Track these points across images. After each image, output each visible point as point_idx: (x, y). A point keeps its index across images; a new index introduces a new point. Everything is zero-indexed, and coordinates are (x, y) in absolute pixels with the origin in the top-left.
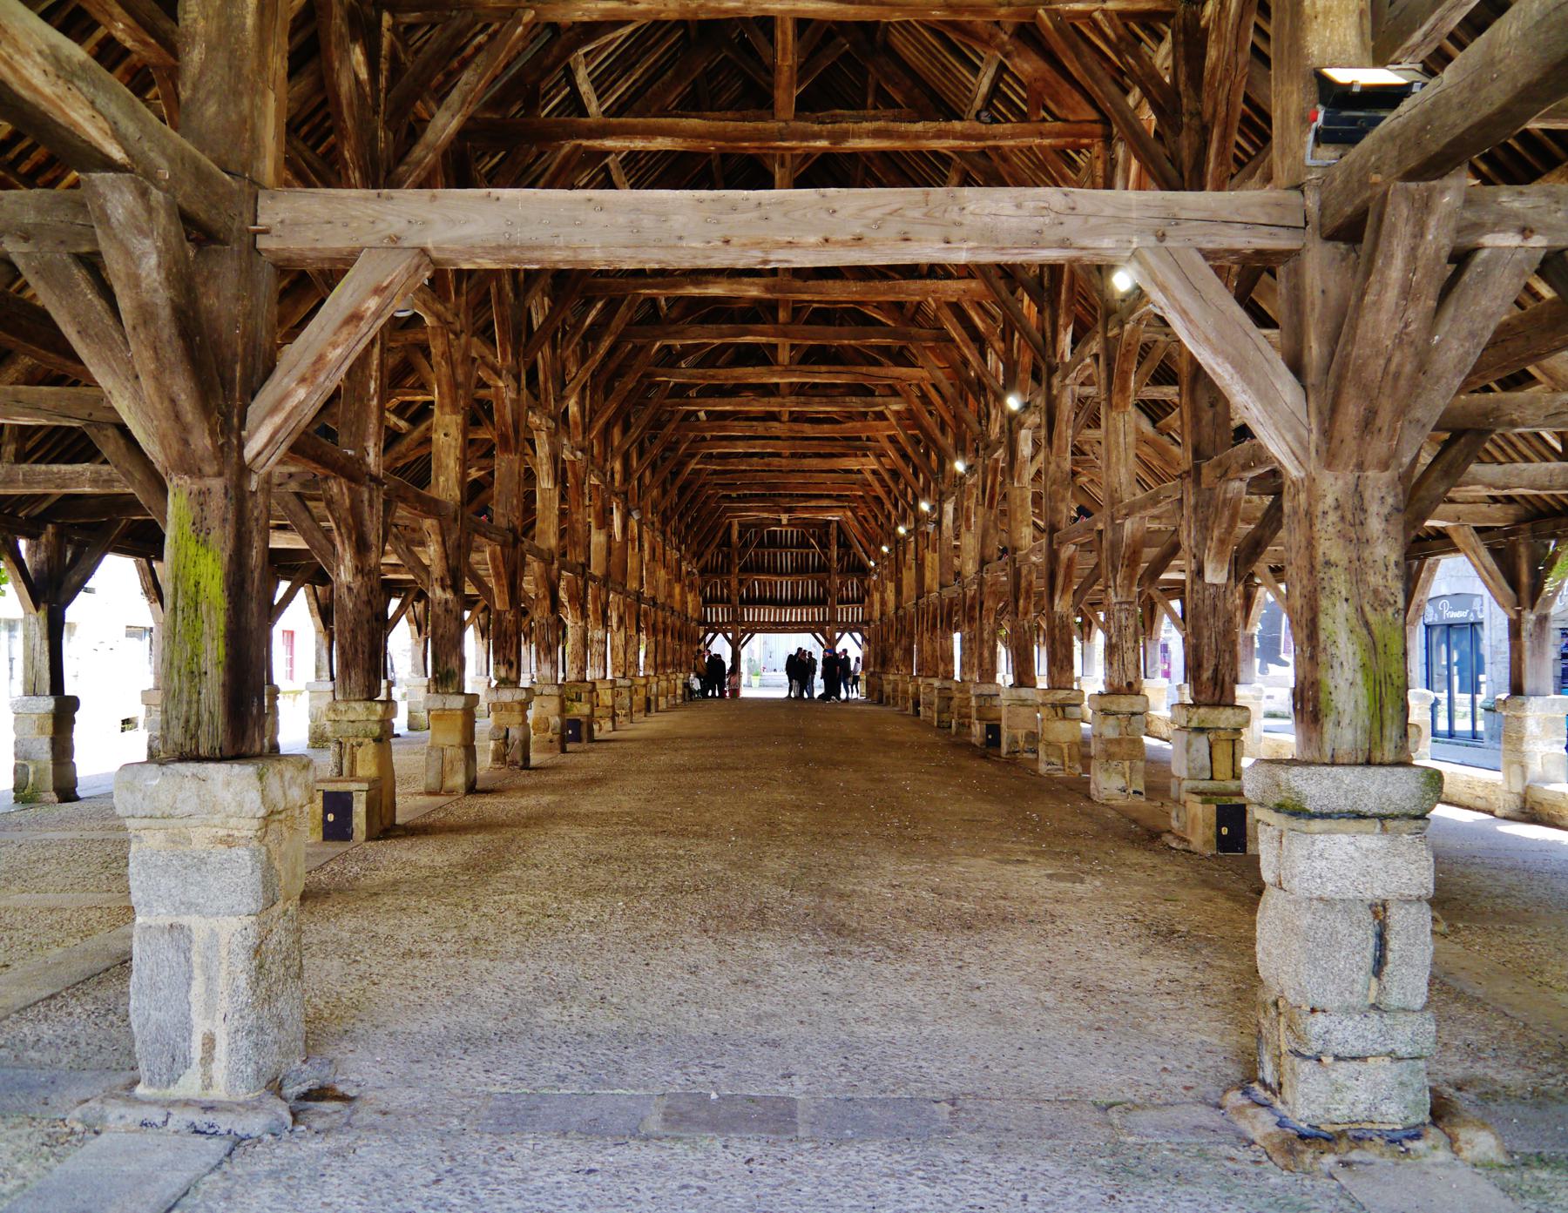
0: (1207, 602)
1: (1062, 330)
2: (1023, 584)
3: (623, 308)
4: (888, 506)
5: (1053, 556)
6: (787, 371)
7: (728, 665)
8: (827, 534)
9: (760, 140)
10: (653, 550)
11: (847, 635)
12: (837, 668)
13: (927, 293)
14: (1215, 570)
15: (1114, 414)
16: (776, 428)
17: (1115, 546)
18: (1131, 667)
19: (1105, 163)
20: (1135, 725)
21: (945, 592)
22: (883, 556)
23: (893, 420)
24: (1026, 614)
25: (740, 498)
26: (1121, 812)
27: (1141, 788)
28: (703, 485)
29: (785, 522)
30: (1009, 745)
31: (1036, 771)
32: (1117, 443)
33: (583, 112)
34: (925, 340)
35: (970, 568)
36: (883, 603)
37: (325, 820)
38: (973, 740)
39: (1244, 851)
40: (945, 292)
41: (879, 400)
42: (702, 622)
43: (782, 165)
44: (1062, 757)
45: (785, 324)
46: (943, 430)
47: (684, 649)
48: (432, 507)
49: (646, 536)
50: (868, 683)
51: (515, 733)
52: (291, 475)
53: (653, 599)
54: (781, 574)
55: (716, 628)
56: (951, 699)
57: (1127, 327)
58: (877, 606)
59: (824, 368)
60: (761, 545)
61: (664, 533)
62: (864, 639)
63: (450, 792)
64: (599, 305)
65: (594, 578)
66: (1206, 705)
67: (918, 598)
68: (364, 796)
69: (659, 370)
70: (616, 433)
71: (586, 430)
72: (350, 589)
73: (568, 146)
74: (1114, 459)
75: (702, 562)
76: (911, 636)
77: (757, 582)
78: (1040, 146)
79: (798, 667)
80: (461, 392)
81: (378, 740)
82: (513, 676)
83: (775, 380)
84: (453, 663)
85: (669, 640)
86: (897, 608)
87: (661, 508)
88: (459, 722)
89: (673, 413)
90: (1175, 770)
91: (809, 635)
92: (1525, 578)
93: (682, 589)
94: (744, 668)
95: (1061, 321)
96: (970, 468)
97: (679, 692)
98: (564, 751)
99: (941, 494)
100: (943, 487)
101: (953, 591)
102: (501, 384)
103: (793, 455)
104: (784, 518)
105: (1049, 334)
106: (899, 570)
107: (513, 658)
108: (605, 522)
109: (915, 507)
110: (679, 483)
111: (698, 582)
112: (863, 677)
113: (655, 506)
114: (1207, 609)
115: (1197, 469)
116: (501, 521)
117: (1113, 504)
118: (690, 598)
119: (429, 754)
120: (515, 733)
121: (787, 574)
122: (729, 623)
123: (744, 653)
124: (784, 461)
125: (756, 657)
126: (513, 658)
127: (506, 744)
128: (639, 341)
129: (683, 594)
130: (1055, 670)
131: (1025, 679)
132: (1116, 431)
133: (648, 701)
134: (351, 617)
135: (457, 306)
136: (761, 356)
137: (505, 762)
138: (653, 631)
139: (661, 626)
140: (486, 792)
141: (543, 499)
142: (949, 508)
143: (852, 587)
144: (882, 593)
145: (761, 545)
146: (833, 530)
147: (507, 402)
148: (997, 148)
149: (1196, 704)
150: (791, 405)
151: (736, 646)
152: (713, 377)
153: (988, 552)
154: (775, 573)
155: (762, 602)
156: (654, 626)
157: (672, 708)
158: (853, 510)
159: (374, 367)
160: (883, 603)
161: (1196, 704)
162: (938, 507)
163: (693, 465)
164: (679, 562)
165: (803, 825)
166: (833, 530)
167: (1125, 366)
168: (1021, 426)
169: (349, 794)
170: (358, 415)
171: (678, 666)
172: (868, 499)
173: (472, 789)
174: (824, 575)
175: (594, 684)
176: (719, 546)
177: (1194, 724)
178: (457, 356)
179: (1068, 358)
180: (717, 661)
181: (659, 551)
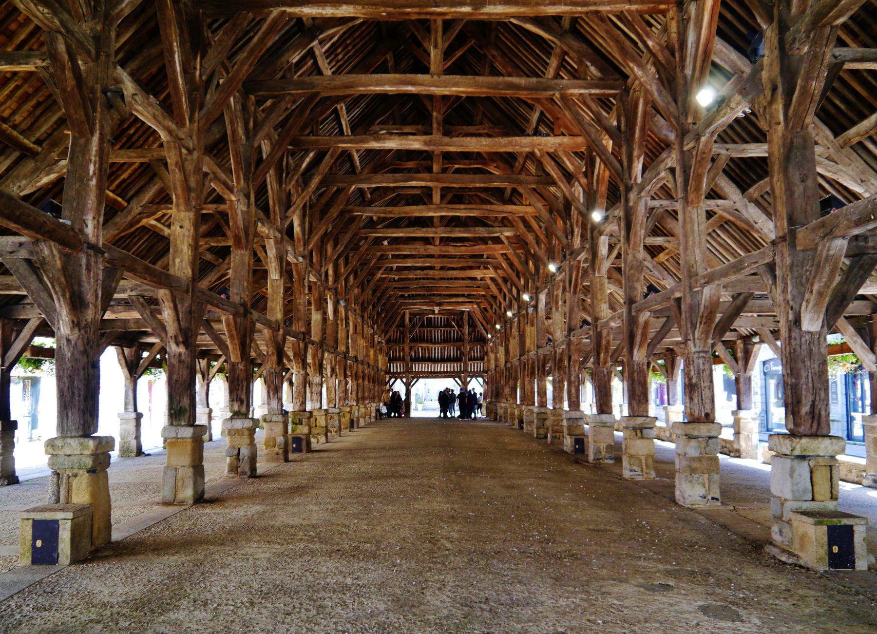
0: (804, 347)
1: (635, 159)
2: (604, 342)
3: (327, 157)
4: (500, 298)
5: (632, 321)
6: (439, 208)
7: (403, 398)
8: (462, 319)
9: (419, 6)
10: (355, 327)
11: (474, 379)
12: (468, 401)
13: (534, 146)
14: (811, 320)
15: (690, 208)
16: (432, 249)
17: (692, 308)
18: (708, 401)
19: (678, 22)
20: (712, 446)
21: (541, 351)
22: (496, 331)
23: (506, 242)
24: (605, 363)
25: (411, 297)
26: (708, 515)
27: (718, 496)
28: (387, 288)
29: (437, 312)
30: (595, 454)
31: (620, 477)
32: (693, 231)
33: (320, 73)
34: (530, 183)
35: (559, 335)
36: (496, 360)
37: (34, 546)
38: (565, 448)
39: (853, 567)
40: (546, 145)
41: (497, 229)
42: (388, 372)
43: (436, 47)
44: (641, 466)
45: (437, 173)
46: (538, 243)
47: (376, 388)
48: (164, 279)
49: (351, 319)
50: (487, 408)
51: (245, 452)
52: (21, 244)
53: (356, 357)
54: (435, 343)
55: (396, 376)
56: (545, 419)
57: (703, 139)
58: (493, 362)
59: (462, 206)
60: (422, 326)
61: (363, 317)
62: (484, 381)
63: (182, 503)
64: (311, 155)
65: (313, 343)
66: (806, 436)
67: (521, 356)
68: (69, 524)
69: (357, 208)
70: (351, 277)
71: (306, 244)
72: (68, 340)
73: (275, 12)
74: (691, 243)
75: (388, 336)
76: (516, 380)
77: (421, 349)
78: (629, 11)
79: (445, 399)
80: (193, 195)
81: (92, 471)
82: (244, 409)
83: (431, 214)
84: (185, 402)
85: (366, 382)
86: (506, 363)
87: (361, 300)
88: (189, 448)
89: (366, 238)
90: (775, 490)
91: (452, 379)
92: (740, 355)
93: (375, 352)
94: (413, 399)
95: (636, 153)
96: (559, 269)
97: (373, 414)
98: (287, 460)
99: (537, 288)
100: (538, 284)
101: (547, 350)
102: (233, 198)
103: (442, 268)
104: (437, 309)
105: (625, 164)
106: (507, 340)
107: (243, 397)
108: (321, 306)
109: (518, 298)
110: (372, 285)
111: (385, 348)
112: (484, 404)
113: (356, 300)
114: (804, 353)
115: (792, 234)
116: (235, 298)
117: (690, 277)
118: (380, 357)
119: (165, 473)
120: (245, 452)
121: (438, 343)
122: (404, 372)
123: (413, 391)
124: (436, 272)
125: (420, 393)
126: (243, 397)
127: (238, 459)
128: (341, 185)
129: (375, 355)
130: (635, 403)
131: (605, 409)
132: (692, 221)
133: (352, 421)
134: (69, 365)
135: (191, 130)
136: (423, 197)
137: (237, 473)
138: (356, 377)
139: (361, 374)
140: (212, 501)
141: (272, 286)
142: (543, 297)
143: (477, 351)
144: (496, 354)
145: (422, 326)
146: (466, 317)
147: (239, 213)
148: (597, 12)
149: (793, 434)
150: (442, 232)
151: (408, 385)
152: (391, 212)
153: (573, 323)
154: (431, 342)
155: (423, 360)
156: (356, 374)
157: (368, 425)
158: (478, 304)
159: (94, 153)
160: (496, 360)
161: (793, 434)
162: (535, 298)
163: (379, 275)
164: (373, 336)
165: (459, 540)
166: (466, 317)
167: (700, 170)
168: (601, 233)
169: (56, 522)
170: (78, 192)
171: (372, 399)
172: (488, 297)
173: (200, 499)
174: (460, 343)
175: (311, 413)
176: (398, 327)
177: (797, 452)
178: (190, 167)
179: (639, 180)
180: (396, 395)
181: (359, 328)
